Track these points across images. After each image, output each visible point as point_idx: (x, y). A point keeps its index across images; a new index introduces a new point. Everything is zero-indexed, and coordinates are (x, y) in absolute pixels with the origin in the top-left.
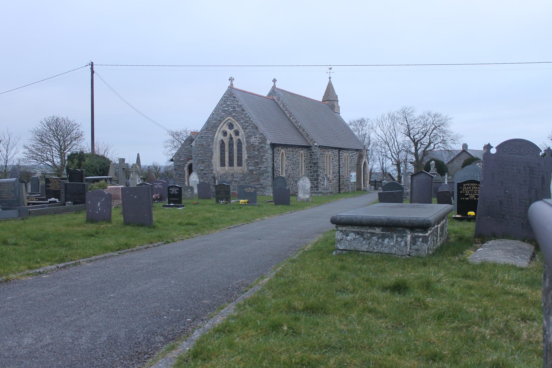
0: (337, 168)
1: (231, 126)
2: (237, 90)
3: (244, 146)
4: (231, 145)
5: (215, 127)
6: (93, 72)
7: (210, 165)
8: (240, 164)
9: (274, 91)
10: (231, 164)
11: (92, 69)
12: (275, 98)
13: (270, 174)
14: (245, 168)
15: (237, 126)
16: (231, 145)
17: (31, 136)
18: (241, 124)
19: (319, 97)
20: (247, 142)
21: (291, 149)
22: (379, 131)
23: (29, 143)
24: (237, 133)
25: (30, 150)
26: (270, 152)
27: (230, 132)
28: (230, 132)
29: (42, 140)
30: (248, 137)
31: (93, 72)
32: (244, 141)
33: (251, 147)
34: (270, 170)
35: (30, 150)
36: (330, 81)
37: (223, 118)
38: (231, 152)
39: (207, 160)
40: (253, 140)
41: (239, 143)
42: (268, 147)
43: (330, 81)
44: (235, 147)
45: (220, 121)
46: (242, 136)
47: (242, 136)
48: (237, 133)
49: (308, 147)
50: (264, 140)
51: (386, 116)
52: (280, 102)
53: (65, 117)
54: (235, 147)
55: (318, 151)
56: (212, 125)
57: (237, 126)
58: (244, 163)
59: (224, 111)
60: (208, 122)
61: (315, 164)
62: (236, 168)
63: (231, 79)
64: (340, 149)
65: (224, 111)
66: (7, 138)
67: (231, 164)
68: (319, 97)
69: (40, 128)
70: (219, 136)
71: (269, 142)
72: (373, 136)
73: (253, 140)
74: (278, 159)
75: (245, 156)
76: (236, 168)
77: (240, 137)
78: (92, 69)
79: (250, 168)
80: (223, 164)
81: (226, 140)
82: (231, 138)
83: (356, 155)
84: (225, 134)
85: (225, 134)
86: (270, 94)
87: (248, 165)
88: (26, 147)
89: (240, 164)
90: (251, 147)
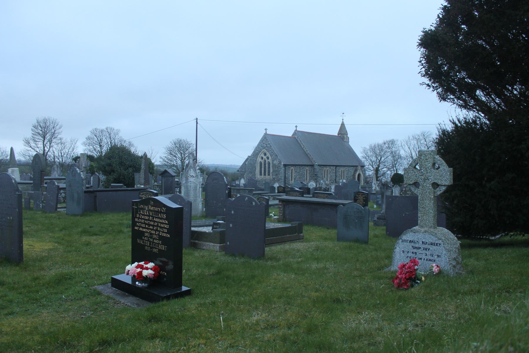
0: (334, 177)
1: (265, 154)
2: (269, 135)
3: (271, 165)
4: (265, 164)
5: (258, 154)
6: (197, 123)
7: (255, 175)
8: (269, 175)
9: (296, 132)
10: (265, 175)
11: (197, 121)
12: (296, 137)
13: (283, 180)
14: (271, 177)
15: (268, 155)
16: (265, 164)
17: (164, 151)
18: (270, 153)
19: (336, 133)
20: (273, 163)
21: (298, 167)
22: (406, 148)
23: (163, 156)
24: (268, 158)
25: (164, 160)
26: (283, 169)
27: (265, 157)
28: (265, 157)
29: (171, 154)
30: (273, 161)
31: (197, 123)
32: (271, 162)
33: (274, 166)
34: (283, 178)
35: (164, 160)
36: (343, 122)
37: (261, 150)
38: (265, 168)
39: (253, 172)
40: (275, 162)
41: (269, 163)
42: (282, 166)
43: (343, 122)
44: (267, 165)
45: (260, 152)
46: (270, 160)
47: (270, 160)
48: (268, 158)
49: (312, 166)
50: (280, 163)
51: (411, 137)
52: (300, 139)
53: (185, 139)
54: (267, 165)
55: (316, 167)
56: (256, 154)
57: (268, 155)
58: (271, 174)
59: (262, 146)
60: (254, 152)
61: (316, 175)
62: (262, 176)
63: (266, 130)
64: (336, 166)
65: (262, 146)
66: (151, 153)
67: (265, 175)
68: (336, 133)
69: (170, 146)
70: (259, 159)
71: (282, 164)
72: (402, 153)
73: (275, 162)
74: (289, 173)
75: (271, 171)
76: (267, 177)
77: (269, 160)
78: (197, 121)
79: (274, 177)
80: (261, 174)
81: (263, 161)
82: (265, 161)
83: (352, 170)
84: (262, 158)
85: (262, 158)
86: (293, 135)
87: (273, 175)
88: (161, 158)
89: (269, 175)
90: (274, 166)
